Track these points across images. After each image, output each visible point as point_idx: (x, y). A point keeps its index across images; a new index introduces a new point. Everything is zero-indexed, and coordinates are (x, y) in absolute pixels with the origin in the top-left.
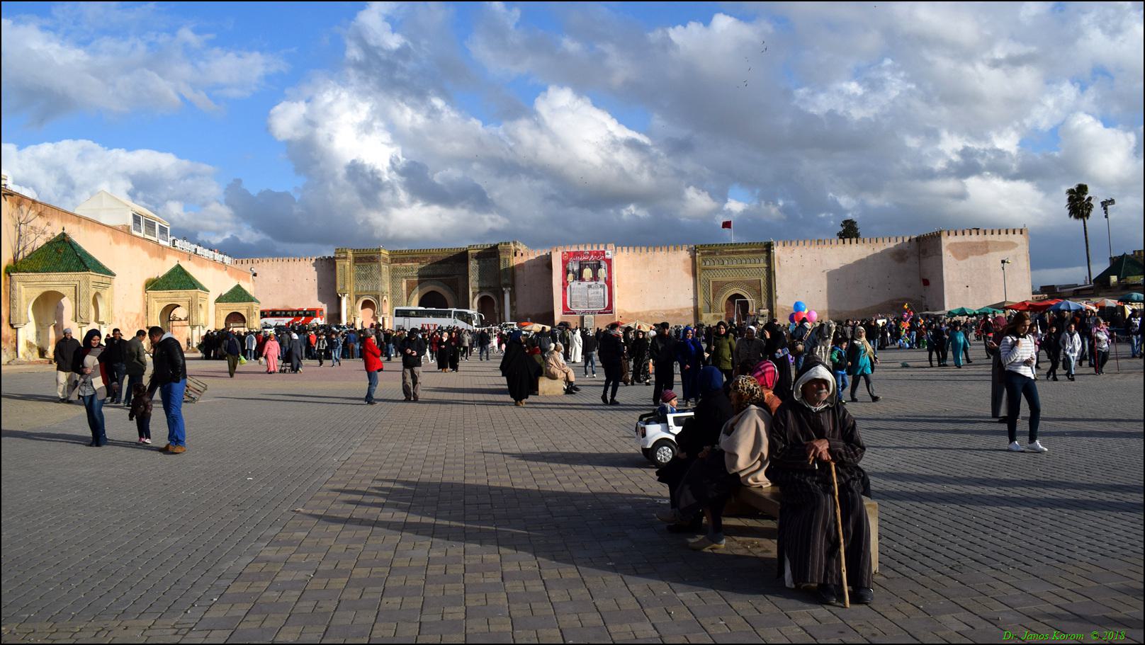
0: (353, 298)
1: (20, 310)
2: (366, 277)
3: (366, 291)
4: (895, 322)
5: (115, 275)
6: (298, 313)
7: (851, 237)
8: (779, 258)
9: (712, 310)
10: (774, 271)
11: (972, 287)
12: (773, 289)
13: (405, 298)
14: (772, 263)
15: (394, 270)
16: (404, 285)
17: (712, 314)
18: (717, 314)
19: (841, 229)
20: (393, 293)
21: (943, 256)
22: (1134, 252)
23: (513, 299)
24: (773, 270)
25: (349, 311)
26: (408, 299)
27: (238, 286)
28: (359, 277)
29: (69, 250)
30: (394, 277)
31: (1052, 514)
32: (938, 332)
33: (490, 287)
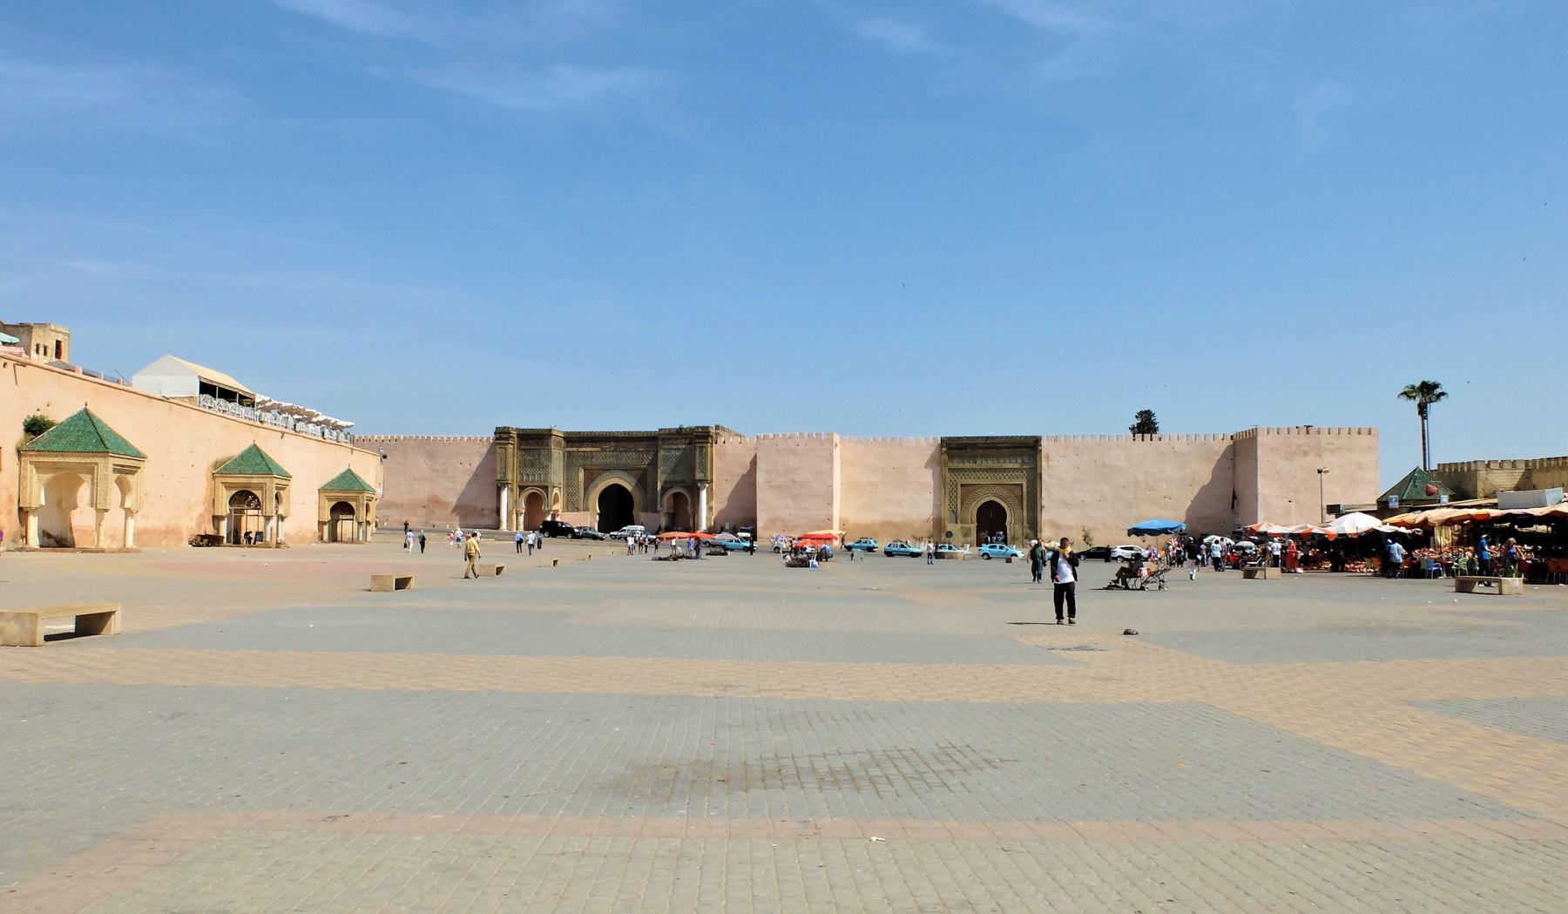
0: (516, 490)
1: (31, 492)
2: (532, 465)
3: (533, 481)
4: (1311, 547)
5: (291, 477)
6: (1244, 551)
7: (1143, 433)
8: (1048, 457)
9: (959, 521)
10: (1041, 474)
11: (1296, 502)
12: (1038, 494)
13: (582, 491)
14: (1038, 463)
15: (569, 456)
16: (581, 474)
17: (959, 525)
18: (965, 525)
19: (1136, 422)
20: (568, 485)
21: (1259, 460)
22: (1439, 465)
23: (710, 498)
24: (1039, 472)
25: (511, 505)
26: (585, 493)
27: (77, 617)
28: (524, 465)
29: (259, 460)
30: (569, 466)
31: (1558, 858)
32: (1193, 556)
33: (683, 482)
